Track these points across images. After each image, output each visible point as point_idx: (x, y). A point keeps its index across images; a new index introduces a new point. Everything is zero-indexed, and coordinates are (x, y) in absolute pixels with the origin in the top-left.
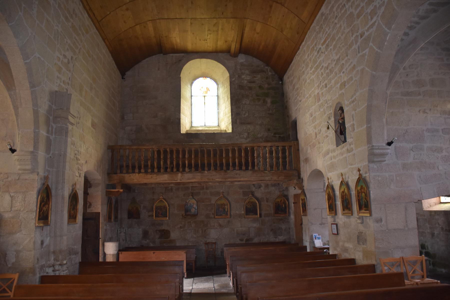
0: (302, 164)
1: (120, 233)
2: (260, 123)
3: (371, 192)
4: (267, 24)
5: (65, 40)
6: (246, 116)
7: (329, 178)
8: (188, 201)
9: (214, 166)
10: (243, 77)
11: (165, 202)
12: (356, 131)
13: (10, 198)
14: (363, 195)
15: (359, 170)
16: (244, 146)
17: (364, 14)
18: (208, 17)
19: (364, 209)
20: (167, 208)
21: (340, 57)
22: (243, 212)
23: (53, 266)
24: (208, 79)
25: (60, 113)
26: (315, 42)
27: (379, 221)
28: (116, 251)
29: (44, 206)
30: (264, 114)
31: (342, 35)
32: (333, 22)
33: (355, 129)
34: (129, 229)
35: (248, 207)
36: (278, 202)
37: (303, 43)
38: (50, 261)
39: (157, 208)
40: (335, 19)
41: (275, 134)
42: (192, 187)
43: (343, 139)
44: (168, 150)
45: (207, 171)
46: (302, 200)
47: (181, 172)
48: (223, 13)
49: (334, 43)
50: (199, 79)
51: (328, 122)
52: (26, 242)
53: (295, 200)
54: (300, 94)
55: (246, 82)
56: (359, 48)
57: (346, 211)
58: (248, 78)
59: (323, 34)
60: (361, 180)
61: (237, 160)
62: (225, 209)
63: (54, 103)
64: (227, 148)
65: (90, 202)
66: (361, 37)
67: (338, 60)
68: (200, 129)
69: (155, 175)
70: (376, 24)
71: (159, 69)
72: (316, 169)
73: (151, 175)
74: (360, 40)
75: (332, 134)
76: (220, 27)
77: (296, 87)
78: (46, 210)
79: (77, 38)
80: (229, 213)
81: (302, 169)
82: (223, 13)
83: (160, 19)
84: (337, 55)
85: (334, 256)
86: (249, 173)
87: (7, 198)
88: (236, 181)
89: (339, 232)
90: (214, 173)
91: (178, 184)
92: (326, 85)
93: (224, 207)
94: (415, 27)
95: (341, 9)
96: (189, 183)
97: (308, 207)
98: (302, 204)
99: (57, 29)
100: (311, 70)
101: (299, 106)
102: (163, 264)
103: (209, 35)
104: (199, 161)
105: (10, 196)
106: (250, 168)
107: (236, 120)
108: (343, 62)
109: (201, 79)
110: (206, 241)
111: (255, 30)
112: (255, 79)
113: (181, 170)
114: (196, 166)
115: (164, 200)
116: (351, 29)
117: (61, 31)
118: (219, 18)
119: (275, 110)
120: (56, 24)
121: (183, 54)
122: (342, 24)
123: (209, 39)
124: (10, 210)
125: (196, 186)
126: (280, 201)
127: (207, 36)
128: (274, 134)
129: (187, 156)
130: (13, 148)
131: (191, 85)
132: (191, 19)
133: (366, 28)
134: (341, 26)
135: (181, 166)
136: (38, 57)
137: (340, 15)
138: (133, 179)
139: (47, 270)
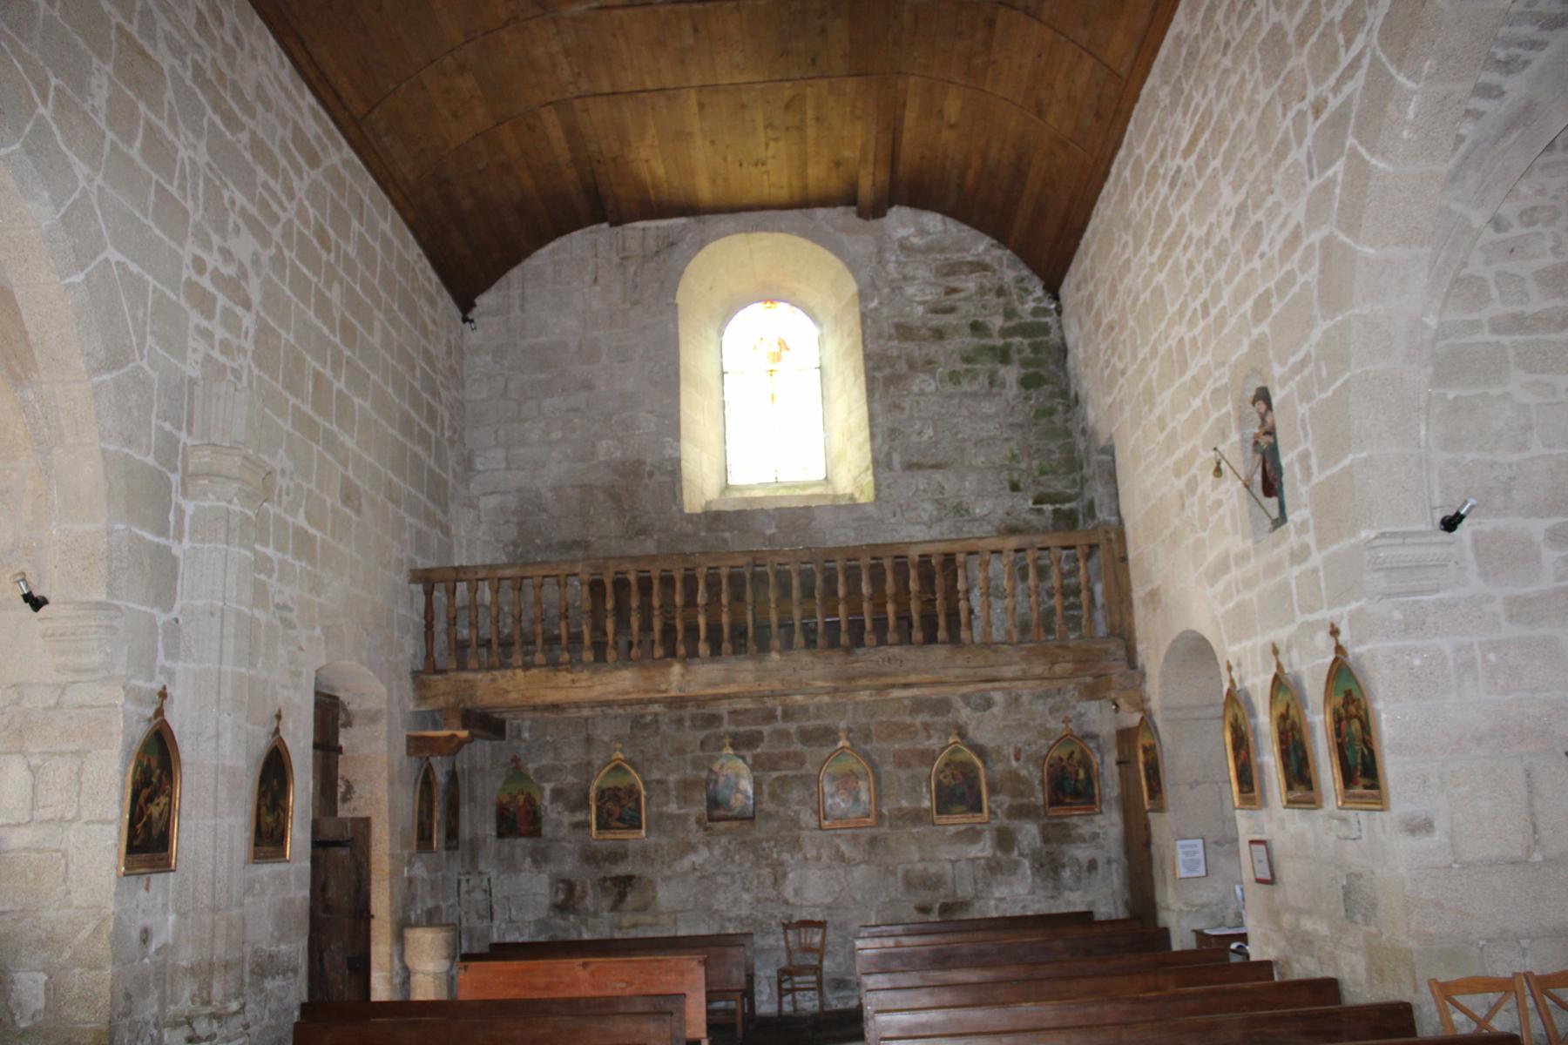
0: (1139, 613)
1: (469, 892)
3: (1384, 716)
4: (983, 91)
5: (226, 194)
6: (925, 438)
7: (1233, 663)
8: (716, 767)
9: (709, 638)
11: (632, 771)
12: (1316, 478)
13: (27, 775)
14: (1353, 727)
15: (1334, 632)
16: (914, 554)
17: (1322, 26)
18: (761, 79)
19: (1362, 781)
20: (639, 794)
21: (1247, 198)
23: (189, 1021)
24: (783, 307)
25: (207, 459)
26: (1161, 145)
27: (1419, 826)
29: (150, 799)
31: (1249, 113)
32: (1216, 66)
33: (1315, 469)
34: (502, 877)
35: (946, 781)
37: (1121, 153)
38: (176, 1004)
40: (1224, 54)
41: (1039, 500)
42: (734, 713)
43: (1275, 514)
44: (632, 577)
45: (780, 652)
46: (1146, 750)
47: (683, 660)
48: (814, 61)
49: (1225, 146)
50: (749, 307)
51: (1215, 449)
52: (84, 934)
53: (1121, 751)
54: (1121, 347)
55: (920, 309)
56: (1309, 159)
57: (1298, 793)
59: (1185, 114)
60: (1341, 671)
61: (890, 608)
63: (184, 425)
64: (827, 565)
66: (1317, 113)
67: (1242, 208)
68: (758, 493)
69: (585, 674)
70: (1366, 61)
72: (1188, 631)
74: (1312, 128)
75: (1231, 493)
76: (810, 114)
77: (1105, 321)
78: (161, 815)
79: (272, 183)
81: (1139, 632)
82: (814, 61)
83: (585, 96)
84: (1236, 189)
85: (1266, 966)
86: (940, 652)
87: (17, 770)
88: (893, 686)
89: (1278, 874)
90: (805, 658)
91: (678, 703)
92: (1205, 306)
94: (1526, 63)
95: (1240, 13)
96: (716, 698)
97: (1168, 778)
98: (1146, 764)
99: (189, 158)
100: (1151, 254)
101: (1120, 390)
102: (603, 1007)
103: (772, 144)
104: (750, 618)
105: (29, 766)
106: (942, 634)
107: (889, 455)
108: (1260, 216)
109: (757, 309)
111: (941, 113)
112: (956, 296)
114: (739, 633)
115: (627, 767)
116: (1280, 87)
117: (208, 164)
118: (802, 78)
120: (187, 139)
121: (681, 221)
122: (1247, 70)
123: (774, 157)
124: (27, 819)
125: (747, 711)
129: (701, 598)
130: (36, 594)
131: (721, 333)
132: (700, 91)
133: (1331, 81)
134: (1243, 80)
135: (680, 636)
136: (118, 263)
137: (1239, 37)
138: (506, 692)
139: (166, 1037)
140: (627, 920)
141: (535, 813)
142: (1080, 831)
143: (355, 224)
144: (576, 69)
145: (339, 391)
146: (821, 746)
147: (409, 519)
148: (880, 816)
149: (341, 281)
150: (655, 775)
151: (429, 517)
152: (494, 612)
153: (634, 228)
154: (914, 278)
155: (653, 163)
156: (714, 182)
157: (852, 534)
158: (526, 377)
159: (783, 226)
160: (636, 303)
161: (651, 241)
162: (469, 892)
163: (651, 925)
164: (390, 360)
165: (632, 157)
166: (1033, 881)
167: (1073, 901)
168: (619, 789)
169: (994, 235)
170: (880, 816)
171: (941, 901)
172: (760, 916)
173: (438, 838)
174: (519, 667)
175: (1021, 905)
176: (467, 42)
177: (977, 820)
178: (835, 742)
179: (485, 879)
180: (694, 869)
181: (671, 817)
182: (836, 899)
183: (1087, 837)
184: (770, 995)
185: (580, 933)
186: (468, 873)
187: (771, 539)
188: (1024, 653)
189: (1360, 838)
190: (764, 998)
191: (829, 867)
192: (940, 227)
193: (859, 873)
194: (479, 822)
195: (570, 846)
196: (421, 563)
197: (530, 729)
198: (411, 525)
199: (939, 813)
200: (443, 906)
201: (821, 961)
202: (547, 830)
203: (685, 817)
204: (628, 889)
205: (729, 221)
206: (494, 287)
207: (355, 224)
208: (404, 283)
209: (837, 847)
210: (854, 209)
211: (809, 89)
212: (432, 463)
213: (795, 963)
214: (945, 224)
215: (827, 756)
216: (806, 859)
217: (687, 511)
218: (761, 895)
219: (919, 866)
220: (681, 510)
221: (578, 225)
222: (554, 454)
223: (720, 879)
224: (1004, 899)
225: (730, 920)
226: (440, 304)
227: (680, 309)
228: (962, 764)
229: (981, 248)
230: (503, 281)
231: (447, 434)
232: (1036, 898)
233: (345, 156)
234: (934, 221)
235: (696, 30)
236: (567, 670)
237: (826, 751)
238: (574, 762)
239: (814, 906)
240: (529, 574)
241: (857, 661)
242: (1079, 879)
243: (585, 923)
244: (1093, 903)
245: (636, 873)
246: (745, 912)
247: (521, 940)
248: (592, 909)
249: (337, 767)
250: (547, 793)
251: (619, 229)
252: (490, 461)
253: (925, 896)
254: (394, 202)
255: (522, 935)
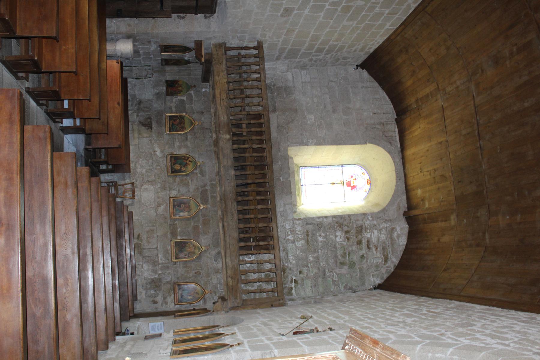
2: (310, 258)
3: (206, 357)
10: (376, 232)
20: (183, 131)
28: (122, 54)
30: (323, 264)
55: (369, 236)
58: (374, 240)
62: (183, 212)
65: (185, 17)
71: (375, 114)
76: (441, 185)
90: (233, 184)
106: (242, 235)
110: (137, 187)
111: (443, 235)
112: (374, 249)
113: (235, 138)
119: (331, 280)
121: (399, 146)
127: (426, 171)
128: (294, 279)
138: (219, 76)
140: (136, 127)
141: (175, 93)
142: (168, 297)
143: (387, 11)
144: (451, 93)
145: (324, 6)
147: (281, 40)
148: (175, 220)
149: (365, 5)
150: (189, 137)
151: (282, 50)
152: (248, 79)
153: (395, 127)
154: (381, 233)
155: (419, 130)
156: (413, 154)
157: (281, 209)
158: (337, 88)
159: (399, 183)
160: (366, 128)
161: (390, 134)
162: (146, 70)
164: (339, 29)
165: (421, 121)
166: (149, 279)
167: (142, 294)
168: (184, 124)
169: (398, 264)
170: (175, 220)
172: (137, 176)
173: (166, 55)
174: (228, 80)
175: (140, 274)
176: (457, 48)
177: (173, 257)
178: (202, 204)
180: (154, 151)
183: (166, 300)
184: (107, 180)
186: (153, 70)
187: (280, 180)
189: (160, 354)
190: (106, 178)
191: (155, 201)
192: (401, 244)
193: (153, 213)
194: (172, 73)
196: (265, 46)
197: (206, 91)
198: (279, 41)
199: (175, 242)
200: (141, 58)
202: (169, 98)
205: (400, 163)
206: (370, 76)
207: (387, 11)
208: (368, 35)
209: (163, 205)
210: (407, 210)
211: (449, 182)
212: (302, 51)
213: (119, 187)
214: (402, 245)
216: (158, 193)
217: (289, 148)
218: (145, 176)
220: (288, 146)
221: (395, 107)
222: (308, 99)
223: (150, 161)
225: (135, 165)
226: (362, 53)
227: (365, 145)
229: (394, 260)
230: (373, 80)
231: (314, 58)
233: (412, 5)
234: (403, 241)
235: (468, 134)
237: (199, 200)
238: (194, 107)
239: (141, 196)
241: (232, 203)
242: (150, 297)
243: (135, 112)
244: (140, 301)
246: (139, 170)
247: (128, 89)
248: (140, 114)
249: (190, 13)
250: (182, 98)
251: (395, 122)
252: (305, 76)
254: (397, 29)
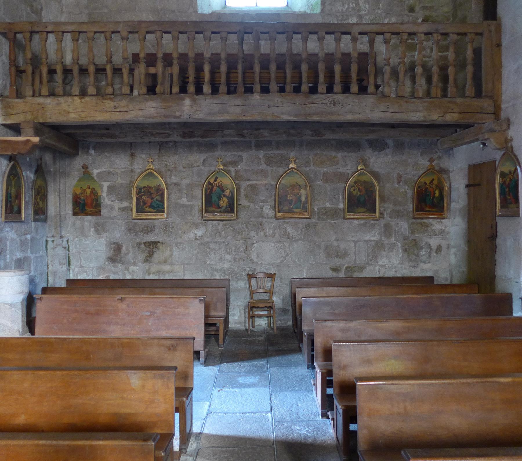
20: (163, 191)
22: (341, 206)
34: (76, 239)
35: (354, 193)
36: (426, 183)
39: (140, 191)
73: (114, 102)
80: (308, 206)
93: (298, 191)
110: (255, 269)
126: (430, 183)
140: (154, 267)
141: (97, 200)
146: (279, 167)
150: (174, 180)
162: (54, 248)
163: (168, 272)
166: (402, 257)
168: (151, 188)
171: (346, 265)
172: (236, 269)
175: (394, 270)
177: (372, 217)
179: (65, 239)
181: (183, 206)
182: (283, 261)
185: (124, 275)
186: (53, 236)
188: (426, 104)
191: (279, 242)
195: (119, 222)
201: (271, 297)
202: (104, 212)
203: (192, 206)
204: (155, 250)
209: (285, 229)
215: (282, 173)
219: (335, 244)
220: (196, 11)
224: (385, 266)
225: (217, 271)
228: (365, 182)
232: (403, 266)
236: (111, 99)
237: (281, 170)
239: (269, 264)
240: (84, 30)
243: (127, 269)
244: (436, 272)
245: (160, 240)
246: (226, 266)
250: (105, 189)
253: (337, 261)
255: (89, 275)
